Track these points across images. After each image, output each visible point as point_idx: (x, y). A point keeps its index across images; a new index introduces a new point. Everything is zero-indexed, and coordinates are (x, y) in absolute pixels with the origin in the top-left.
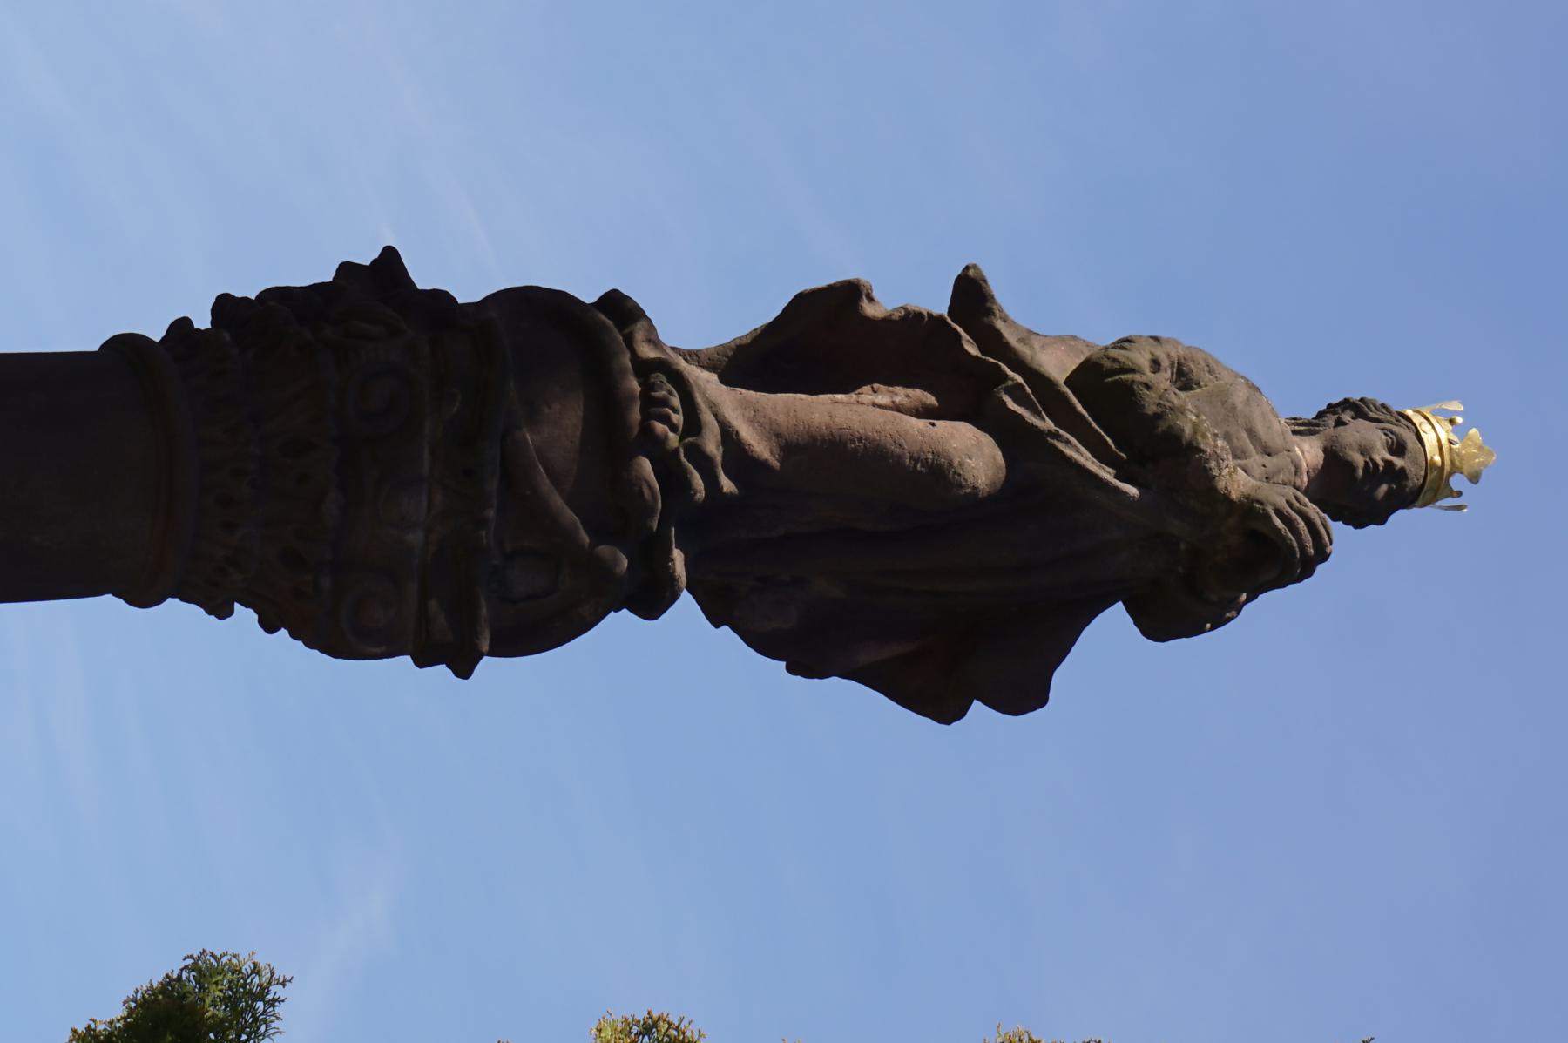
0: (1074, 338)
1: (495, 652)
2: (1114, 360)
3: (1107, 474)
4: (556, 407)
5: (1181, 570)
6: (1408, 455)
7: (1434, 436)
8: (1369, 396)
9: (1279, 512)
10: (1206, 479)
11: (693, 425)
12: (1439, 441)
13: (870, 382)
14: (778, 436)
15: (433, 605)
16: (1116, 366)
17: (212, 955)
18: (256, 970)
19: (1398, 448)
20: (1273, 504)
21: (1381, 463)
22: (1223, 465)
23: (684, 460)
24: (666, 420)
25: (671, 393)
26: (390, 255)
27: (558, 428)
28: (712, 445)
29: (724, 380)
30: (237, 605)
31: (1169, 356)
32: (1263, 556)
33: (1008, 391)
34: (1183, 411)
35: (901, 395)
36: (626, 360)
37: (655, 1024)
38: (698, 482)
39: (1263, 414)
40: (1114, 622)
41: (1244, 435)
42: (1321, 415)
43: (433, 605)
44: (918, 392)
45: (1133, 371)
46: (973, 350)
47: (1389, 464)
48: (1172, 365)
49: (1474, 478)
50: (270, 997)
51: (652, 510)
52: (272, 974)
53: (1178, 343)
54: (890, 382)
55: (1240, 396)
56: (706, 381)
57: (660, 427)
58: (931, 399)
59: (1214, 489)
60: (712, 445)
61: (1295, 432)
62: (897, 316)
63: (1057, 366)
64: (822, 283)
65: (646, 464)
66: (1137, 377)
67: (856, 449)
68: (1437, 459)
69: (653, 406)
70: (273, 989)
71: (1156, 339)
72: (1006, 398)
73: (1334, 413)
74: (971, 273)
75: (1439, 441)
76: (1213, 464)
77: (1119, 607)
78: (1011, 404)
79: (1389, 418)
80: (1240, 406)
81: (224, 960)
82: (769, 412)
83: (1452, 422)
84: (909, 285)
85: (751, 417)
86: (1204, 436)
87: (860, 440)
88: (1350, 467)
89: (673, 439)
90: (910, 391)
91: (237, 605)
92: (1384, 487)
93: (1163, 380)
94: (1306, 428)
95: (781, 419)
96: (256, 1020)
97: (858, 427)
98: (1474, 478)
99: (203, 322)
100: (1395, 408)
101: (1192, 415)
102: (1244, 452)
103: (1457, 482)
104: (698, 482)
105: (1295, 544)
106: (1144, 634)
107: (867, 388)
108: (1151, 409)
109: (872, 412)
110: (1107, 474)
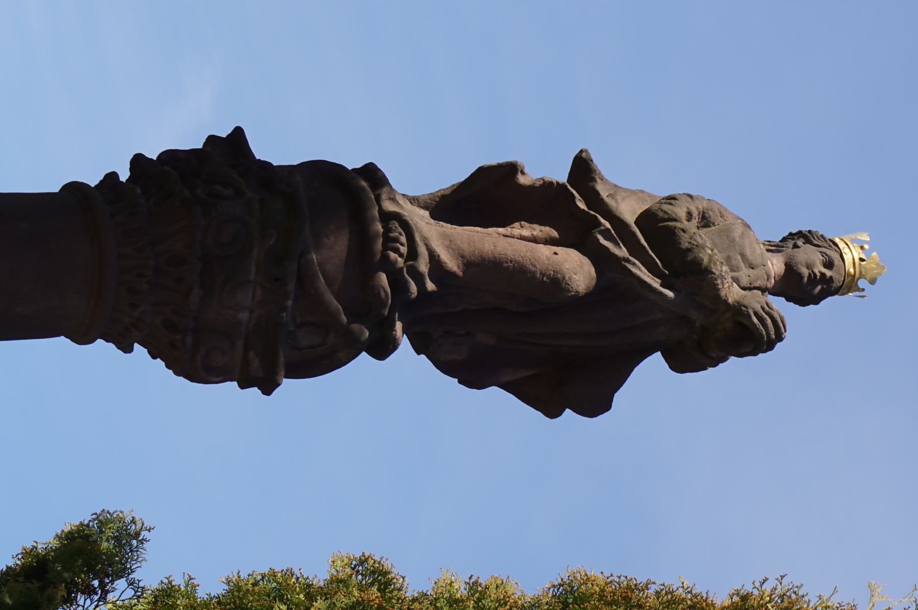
0: (642, 191)
1: (288, 376)
2: (665, 212)
3: (655, 283)
4: (332, 238)
5: (695, 337)
6: (835, 268)
7: (851, 255)
8: (814, 230)
9: (756, 314)
10: (715, 289)
11: (413, 254)
12: (854, 259)
13: (519, 220)
14: (463, 257)
15: (252, 354)
16: (666, 216)
17: (108, 512)
18: (133, 521)
19: (829, 265)
20: (753, 309)
21: (818, 274)
22: (725, 282)
23: (406, 275)
24: (397, 251)
25: (400, 234)
26: (238, 133)
27: (332, 251)
28: (423, 266)
29: (433, 216)
30: (136, 345)
31: (697, 208)
32: (749, 336)
33: (601, 233)
34: (703, 247)
35: (538, 230)
36: (376, 212)
37: (366, 560)
38: (413, 288)
39: (751, 243)
40: (656, 360)
41: (739, 257)
42: (784, 240)
43: (252, 354)
44: (548, 228)
45: (675, 220)
46: (582, 205)
47: (823, 274)
48: (699, 214)
49: (873, 282)
50: (141, 538)
51: (386, 304)
52: (143, 524)
53: (703, 198)
54: (531, 221)
55: (738, 231)
56: (420, 218)
57: (393, 255)
58: (555, 234)
59: (719, 296)
60: (423, 266)
61: (768, 250)
62: (538, 184)
63: (629, 212)
64: (494, 162)
65: (383, 278)
66: (678, 225)
67: (508, 267)
68: (852, 270)
69: (390, 242)
70: (143, 533)
71: (691, 196)
72: (599, 237)
73: (793, 239)
74: (584, 155)
75: (854, 259)
76: (719, 281)
77: (658, 355)
78: (602, 241)
79: (826, 245)
80: (737, 239)
81: (115, 515)
82: (458, 242)
83: (862, 248)
84: (546, 166)
85: (447, 243)
86: (715, 264)
87: (511, 262)
88: (800, 276)
89: (400, 261)
90: (543, 228)
91: (136, 345)
92: (819, 287)
93: (692, 226)
94: (775, 248)
95: (465, 247)
96: (131, 551)
97: (510, 254)
98: (873, 282)
99: (124, 175)
100: (828, 236)
101: (708, 247)
102: (738, 268)
103: (862, 283)
104: (413, 288)
105: (764, 333)
106: (670, 368)
107: (517, 224)
108: (685, 245)
109: (518, 243)
110: (655, 283)
